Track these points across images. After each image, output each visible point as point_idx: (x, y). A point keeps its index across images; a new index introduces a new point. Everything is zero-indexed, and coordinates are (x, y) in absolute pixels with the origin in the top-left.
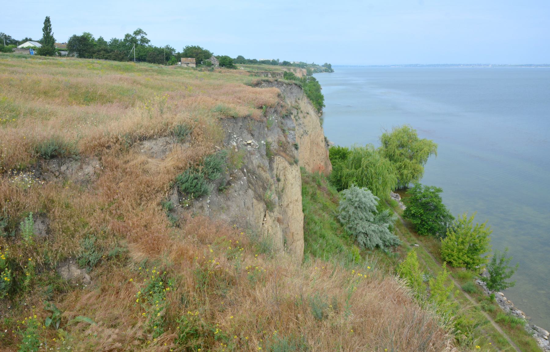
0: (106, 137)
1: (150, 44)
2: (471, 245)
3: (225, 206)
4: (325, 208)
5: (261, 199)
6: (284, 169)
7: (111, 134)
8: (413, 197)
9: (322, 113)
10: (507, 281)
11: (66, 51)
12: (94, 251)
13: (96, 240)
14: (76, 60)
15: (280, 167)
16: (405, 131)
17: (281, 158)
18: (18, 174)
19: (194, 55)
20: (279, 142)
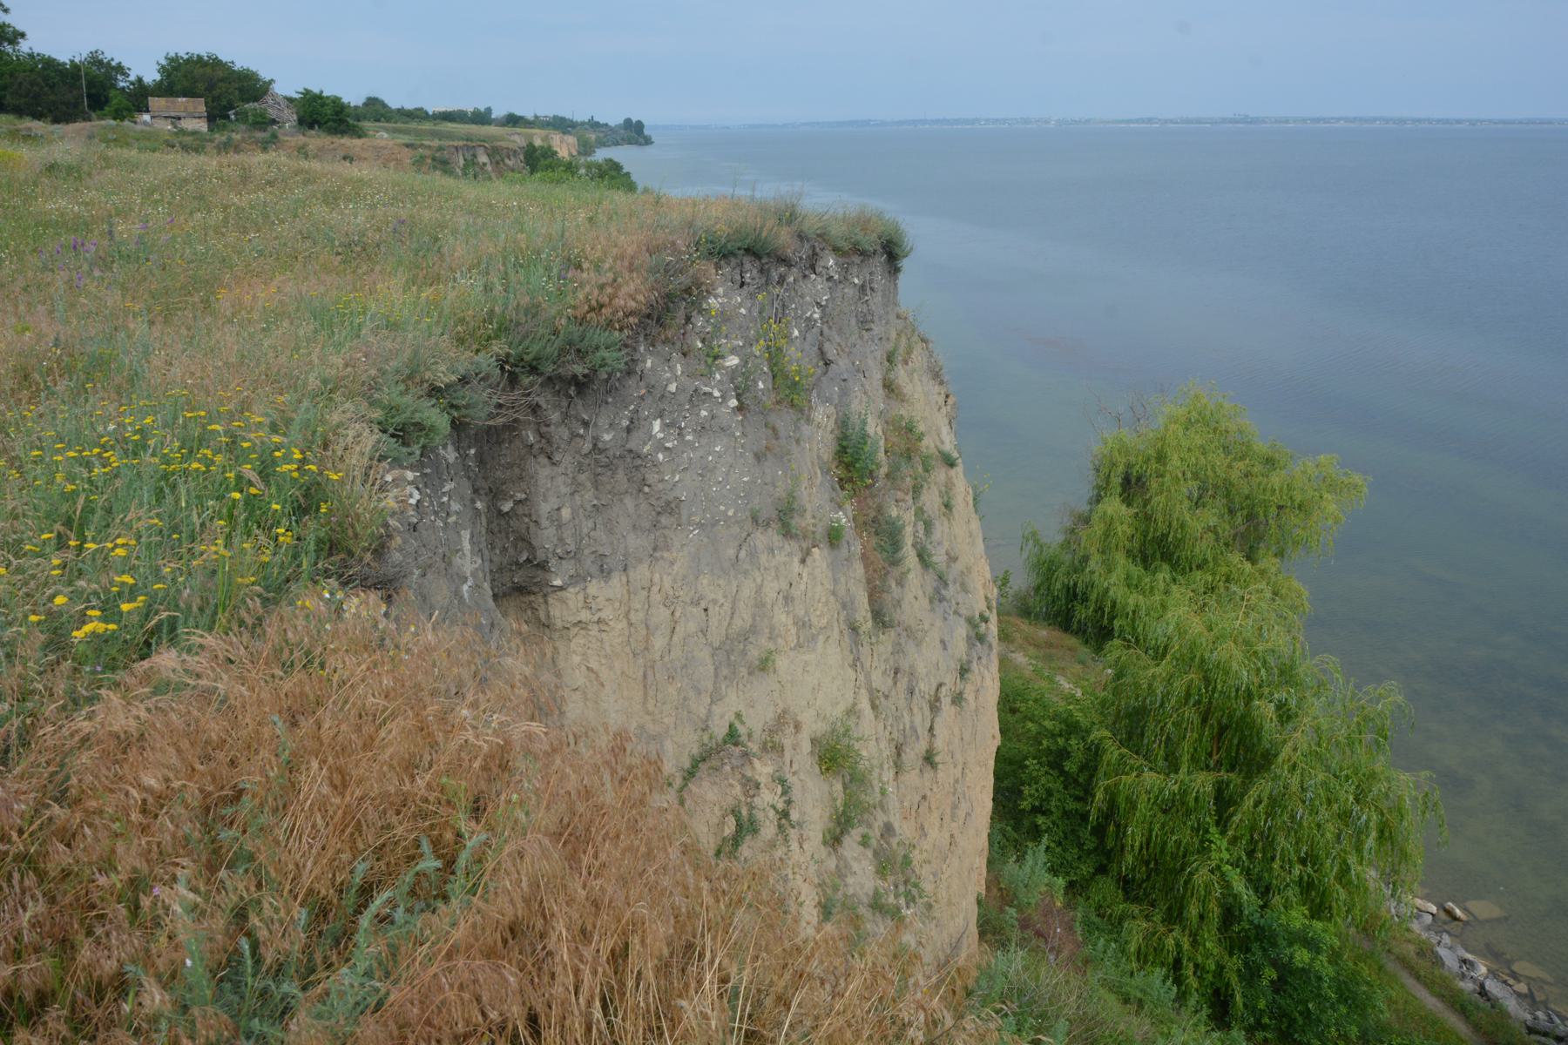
1: (24, 47)
19: (201, 86)
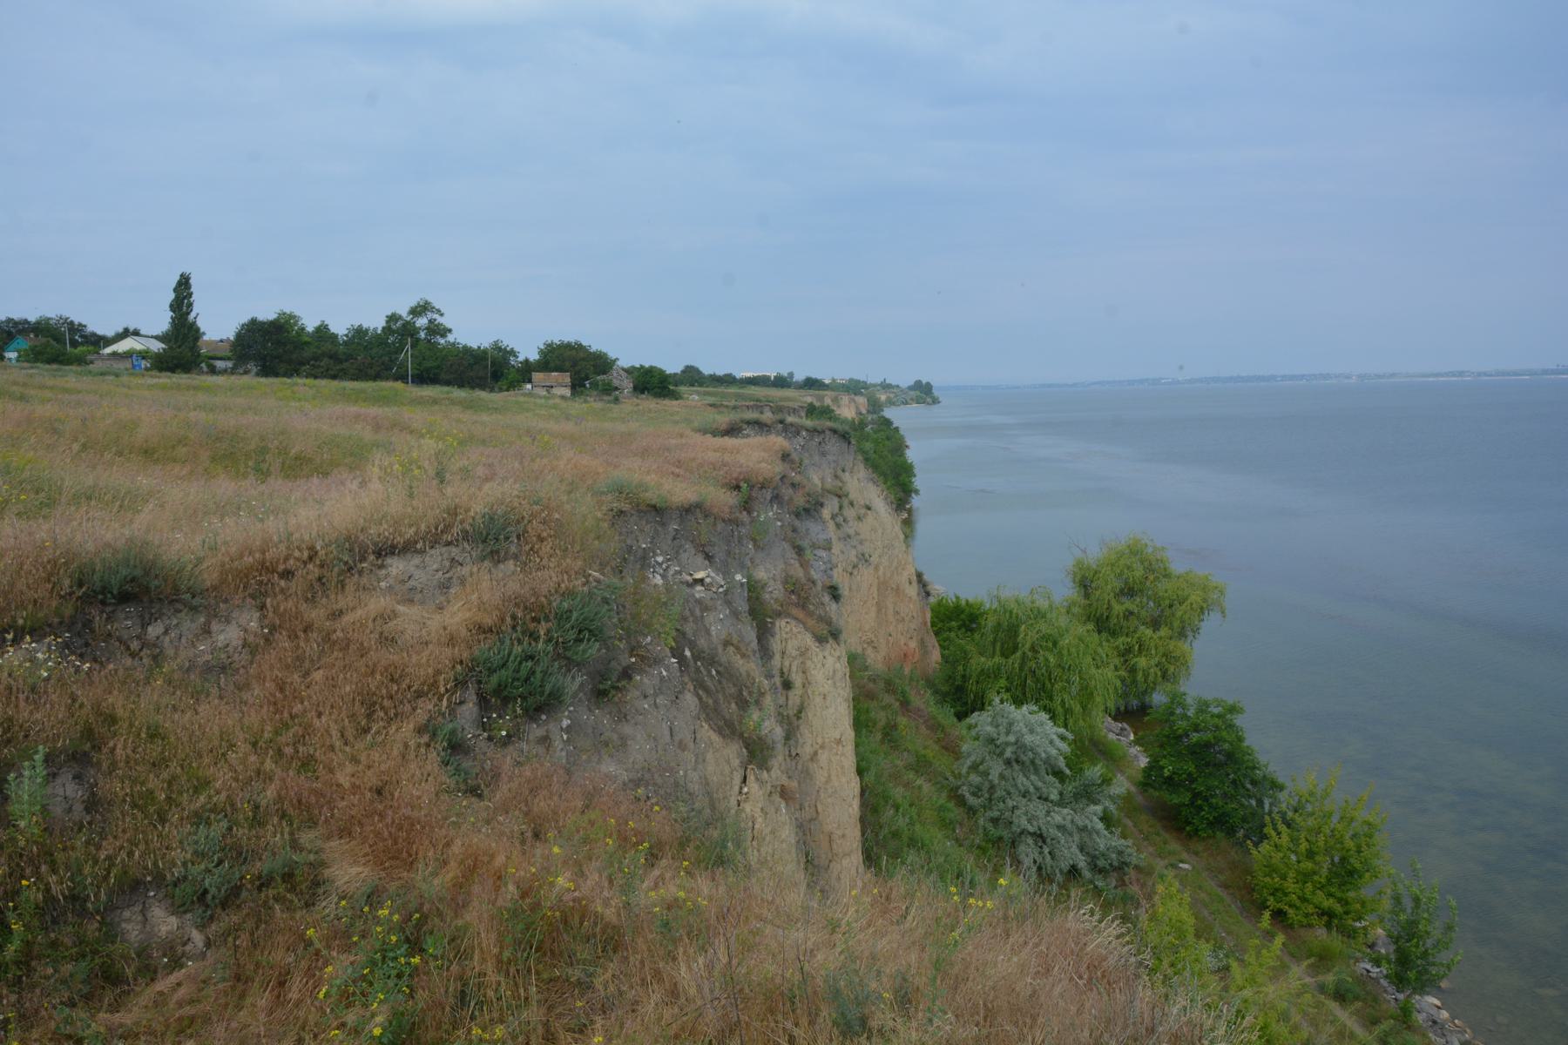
0: (282, 547)
1: (450, 338)
2: (1337, 859)
3: (615, 737)
4: (921, 765)
5: (733, 733)
6: (802, 654)
7: (297, 535)
8: (1166, 731)
9: (910, 511)
10: (1443, 957)
11: (229, 359)
12: (220, 862)
13: (230, 829)
14: (250, 380)
15: (792, 648)
16: (1135, 550)
17: (793, 623)
18: (16, 641)
19: (568, 364)
20: (786, 581)
